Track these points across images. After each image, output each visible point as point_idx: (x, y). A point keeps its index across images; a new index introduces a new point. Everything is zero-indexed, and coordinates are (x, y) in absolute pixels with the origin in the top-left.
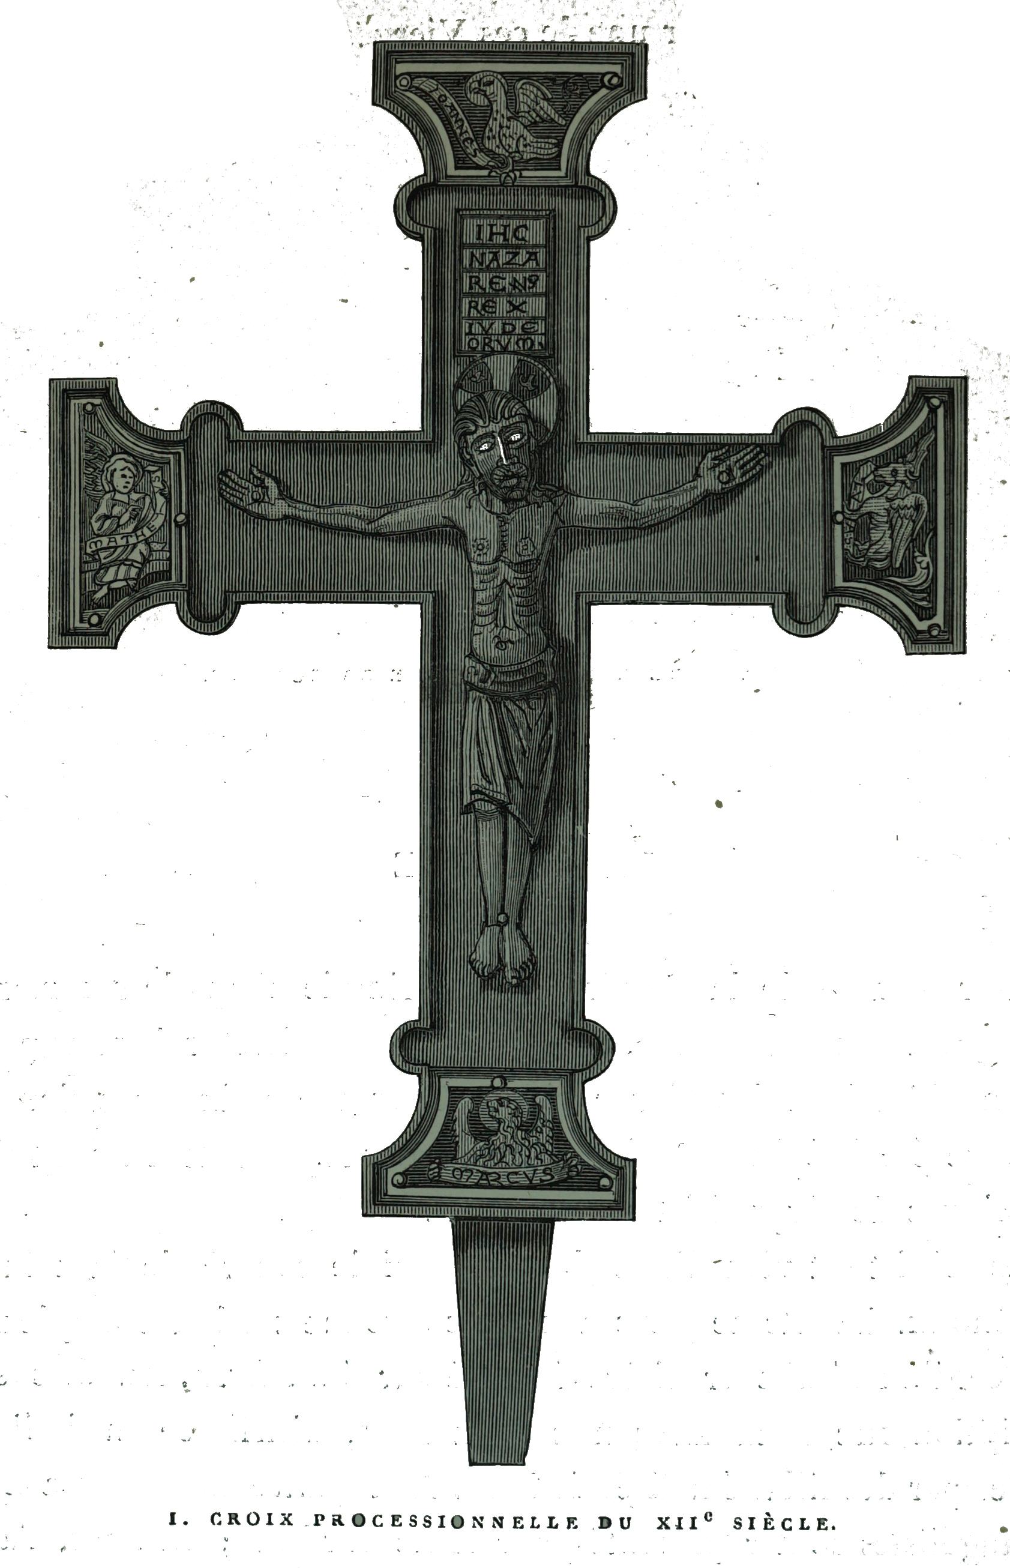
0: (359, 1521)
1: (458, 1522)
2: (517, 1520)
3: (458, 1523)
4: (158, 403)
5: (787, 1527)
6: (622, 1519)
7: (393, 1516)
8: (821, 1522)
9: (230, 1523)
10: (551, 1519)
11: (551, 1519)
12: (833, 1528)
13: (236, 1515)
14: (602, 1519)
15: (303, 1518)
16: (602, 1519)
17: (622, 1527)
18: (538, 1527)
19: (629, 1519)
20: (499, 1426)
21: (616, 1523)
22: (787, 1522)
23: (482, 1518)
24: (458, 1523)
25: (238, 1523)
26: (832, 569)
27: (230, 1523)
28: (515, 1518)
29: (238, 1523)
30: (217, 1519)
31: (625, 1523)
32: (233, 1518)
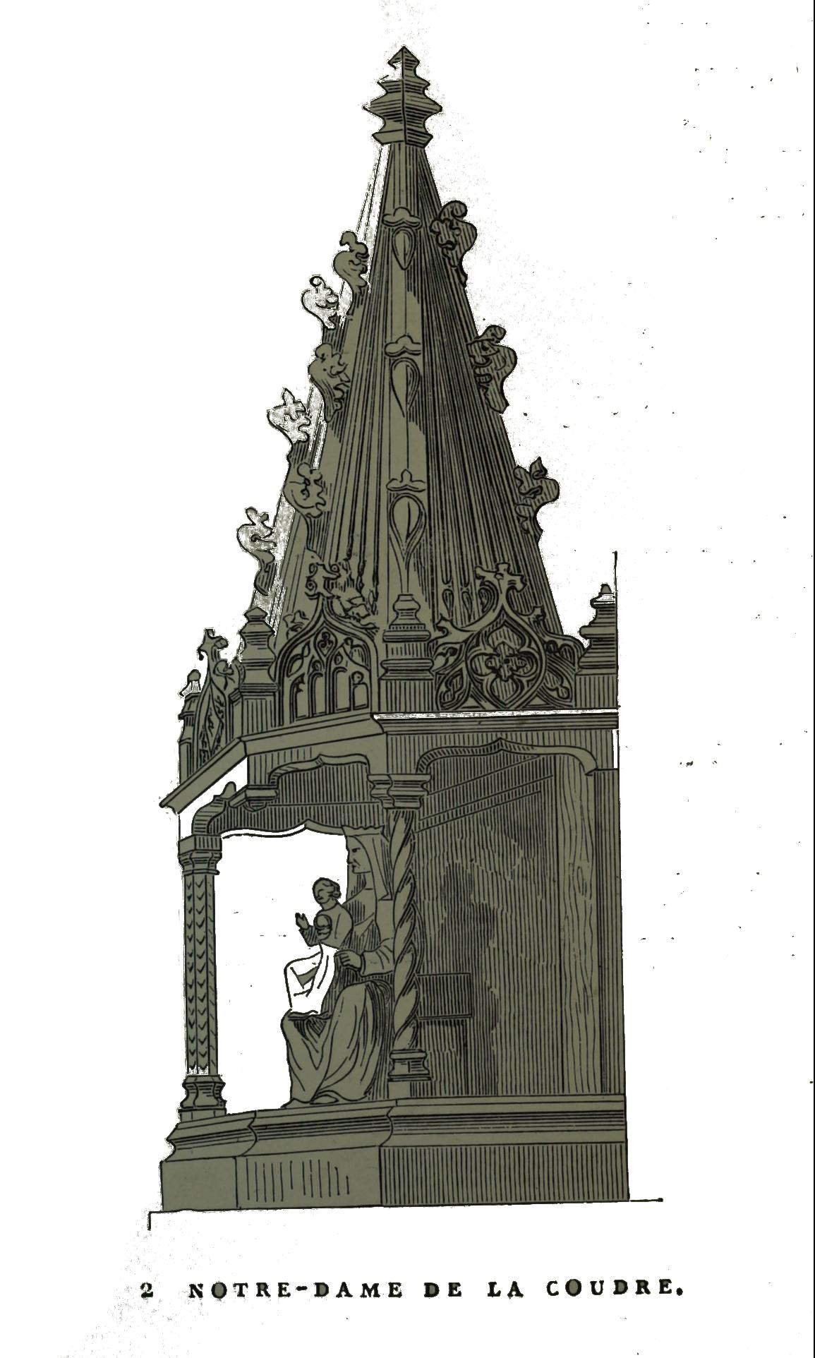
0: (574, 1288)
1: (574, 1288)
2: (282, 1287)
3: (573, 1289)
4: (432, 124)
5: (553, 1291)
6: (593, 1283)
7: (451, 1284)
8: (664, 1283)
9: (639, 1292)
10: (492, 1285)
11: (492, 1285)
12: (680, 1292)
13: (646, 1283)
14: (428, 1285)
15: (533, 1288)
16: (428, 1285)
17: (594, 1292)
18: (499, 1294)
19: (602, 1282)
20: (149, 1228)
21: (586, 1288)
22: (553, 1286)
23: (201, 1286)
24: (573, 1289)
25: (268, 1295)
26: (291, 704)
27: (639, 1292)
28: (280, 1285)
29: (268, 1295)
30: (553, 1288)
31: (196, 1291)
32: (642, 1286)
